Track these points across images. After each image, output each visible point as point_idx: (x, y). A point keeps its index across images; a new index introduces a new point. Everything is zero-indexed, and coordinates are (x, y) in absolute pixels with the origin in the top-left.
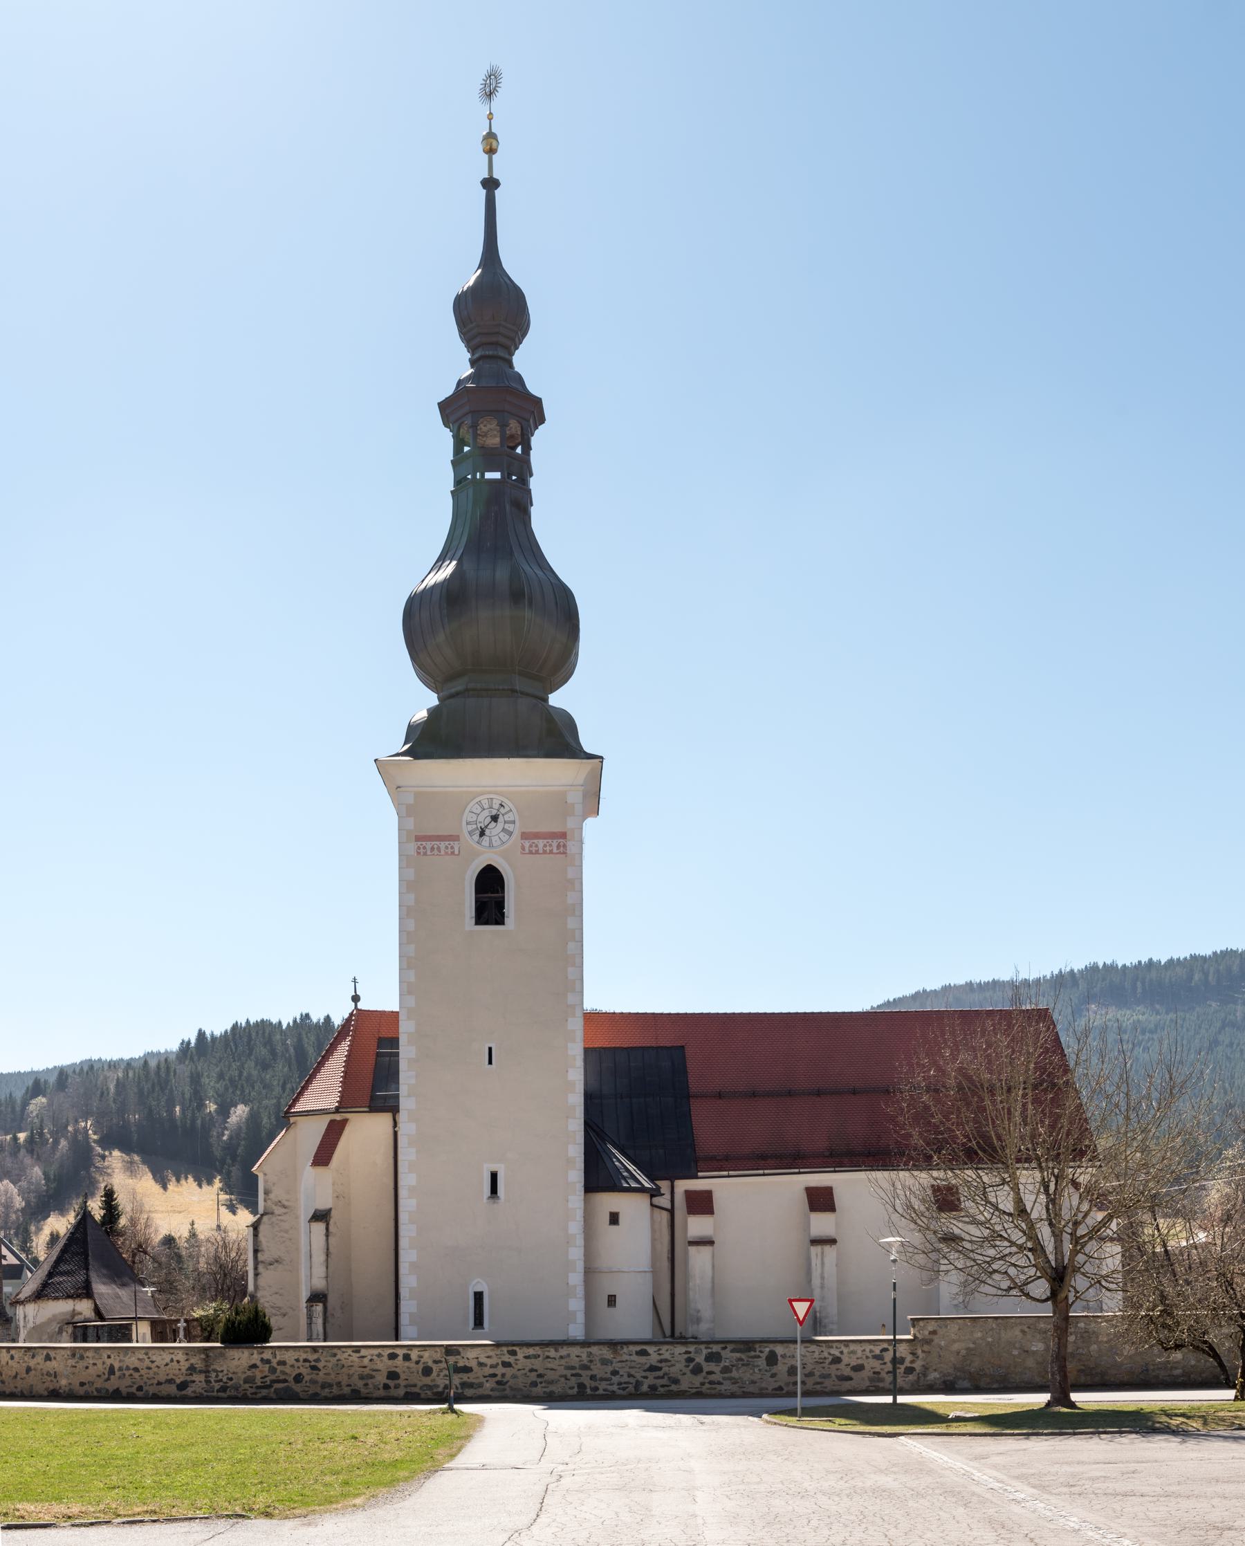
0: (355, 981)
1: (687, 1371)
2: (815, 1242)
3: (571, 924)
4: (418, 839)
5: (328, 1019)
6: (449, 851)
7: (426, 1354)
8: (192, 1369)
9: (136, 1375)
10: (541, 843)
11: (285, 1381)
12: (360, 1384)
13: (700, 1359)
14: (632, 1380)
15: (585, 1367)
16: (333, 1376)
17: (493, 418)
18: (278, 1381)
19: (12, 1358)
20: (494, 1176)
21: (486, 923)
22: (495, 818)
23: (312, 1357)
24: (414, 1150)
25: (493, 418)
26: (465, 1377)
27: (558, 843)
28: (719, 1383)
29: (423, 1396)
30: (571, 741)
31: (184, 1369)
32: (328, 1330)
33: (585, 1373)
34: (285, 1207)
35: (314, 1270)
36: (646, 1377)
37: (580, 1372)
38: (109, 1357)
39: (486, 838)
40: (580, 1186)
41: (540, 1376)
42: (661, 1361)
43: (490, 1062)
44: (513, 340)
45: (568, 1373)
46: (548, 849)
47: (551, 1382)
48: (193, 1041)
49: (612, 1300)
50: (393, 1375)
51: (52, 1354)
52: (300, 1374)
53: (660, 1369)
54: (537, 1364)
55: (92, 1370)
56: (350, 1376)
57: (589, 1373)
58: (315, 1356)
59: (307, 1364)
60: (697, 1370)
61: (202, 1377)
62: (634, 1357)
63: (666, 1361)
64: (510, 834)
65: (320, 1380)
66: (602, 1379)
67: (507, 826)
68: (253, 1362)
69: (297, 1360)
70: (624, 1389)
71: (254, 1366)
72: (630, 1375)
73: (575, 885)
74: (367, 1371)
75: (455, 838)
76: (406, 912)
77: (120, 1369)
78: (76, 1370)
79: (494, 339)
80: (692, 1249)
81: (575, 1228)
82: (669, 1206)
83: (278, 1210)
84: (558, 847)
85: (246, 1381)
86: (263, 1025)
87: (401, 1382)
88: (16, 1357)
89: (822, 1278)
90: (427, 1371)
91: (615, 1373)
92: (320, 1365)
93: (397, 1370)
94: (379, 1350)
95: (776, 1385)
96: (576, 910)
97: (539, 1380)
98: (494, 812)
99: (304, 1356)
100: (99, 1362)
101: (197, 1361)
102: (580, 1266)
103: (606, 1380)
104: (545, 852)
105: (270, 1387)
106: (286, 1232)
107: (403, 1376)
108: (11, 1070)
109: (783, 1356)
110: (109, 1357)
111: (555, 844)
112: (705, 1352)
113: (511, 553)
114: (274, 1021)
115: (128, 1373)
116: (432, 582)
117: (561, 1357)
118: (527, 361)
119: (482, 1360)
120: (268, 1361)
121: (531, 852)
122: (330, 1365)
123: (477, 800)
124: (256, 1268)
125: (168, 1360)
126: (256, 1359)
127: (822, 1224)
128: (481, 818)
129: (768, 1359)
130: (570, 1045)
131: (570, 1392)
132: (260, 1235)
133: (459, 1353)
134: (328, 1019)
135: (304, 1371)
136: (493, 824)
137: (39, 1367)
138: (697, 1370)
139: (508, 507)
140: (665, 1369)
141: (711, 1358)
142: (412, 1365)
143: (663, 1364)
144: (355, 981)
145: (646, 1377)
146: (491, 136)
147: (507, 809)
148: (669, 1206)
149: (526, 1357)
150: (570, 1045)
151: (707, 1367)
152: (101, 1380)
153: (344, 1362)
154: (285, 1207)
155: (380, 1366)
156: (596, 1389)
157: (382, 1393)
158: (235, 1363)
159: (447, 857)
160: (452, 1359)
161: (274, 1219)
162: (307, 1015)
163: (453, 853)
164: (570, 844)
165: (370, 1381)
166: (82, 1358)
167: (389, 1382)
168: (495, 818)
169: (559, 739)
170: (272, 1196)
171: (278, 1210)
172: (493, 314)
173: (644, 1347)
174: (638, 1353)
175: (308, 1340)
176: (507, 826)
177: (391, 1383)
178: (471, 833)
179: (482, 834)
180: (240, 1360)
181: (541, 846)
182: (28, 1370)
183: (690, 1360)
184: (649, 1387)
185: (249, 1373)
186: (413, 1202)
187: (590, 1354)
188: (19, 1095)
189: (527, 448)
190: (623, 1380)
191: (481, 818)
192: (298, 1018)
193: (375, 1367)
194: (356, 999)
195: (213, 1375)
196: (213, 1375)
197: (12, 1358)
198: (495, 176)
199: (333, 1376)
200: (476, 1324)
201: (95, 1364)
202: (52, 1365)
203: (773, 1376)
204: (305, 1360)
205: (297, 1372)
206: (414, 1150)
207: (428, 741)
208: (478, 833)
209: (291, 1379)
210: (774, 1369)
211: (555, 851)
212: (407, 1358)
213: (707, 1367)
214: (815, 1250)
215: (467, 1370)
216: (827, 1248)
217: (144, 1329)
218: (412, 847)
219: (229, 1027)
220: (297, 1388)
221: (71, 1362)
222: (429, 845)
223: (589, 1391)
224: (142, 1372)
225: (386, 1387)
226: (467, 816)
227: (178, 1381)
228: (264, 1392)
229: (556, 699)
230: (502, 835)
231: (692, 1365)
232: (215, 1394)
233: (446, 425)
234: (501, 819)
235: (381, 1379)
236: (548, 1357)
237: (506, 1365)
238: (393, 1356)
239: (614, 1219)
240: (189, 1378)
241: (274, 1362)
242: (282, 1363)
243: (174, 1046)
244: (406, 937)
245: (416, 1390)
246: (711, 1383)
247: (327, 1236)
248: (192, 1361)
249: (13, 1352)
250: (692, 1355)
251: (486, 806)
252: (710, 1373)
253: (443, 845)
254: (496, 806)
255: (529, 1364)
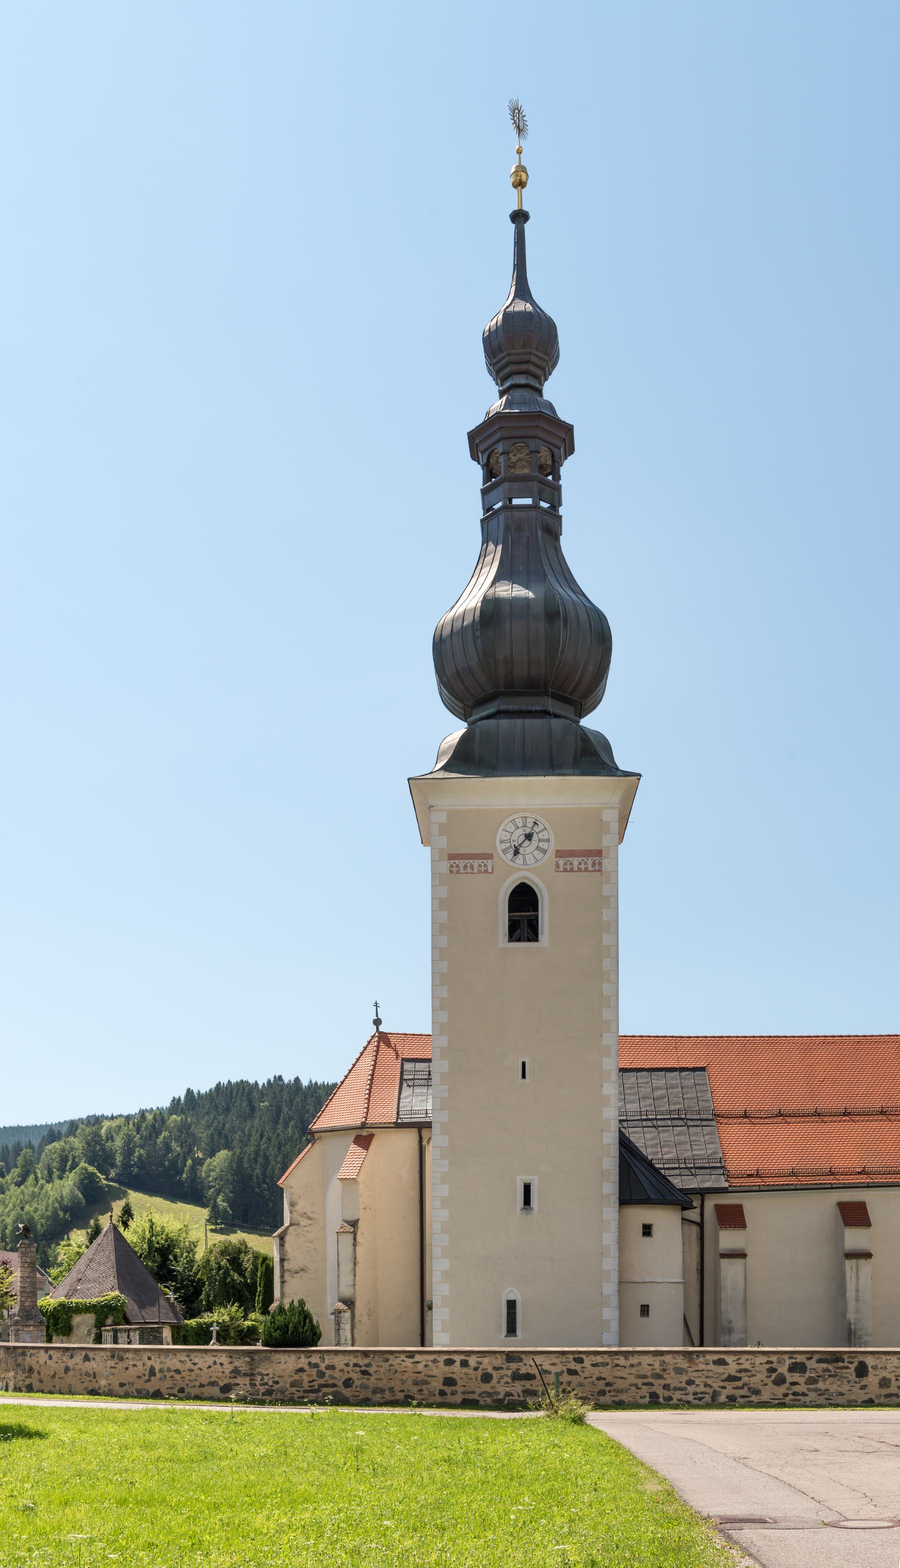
0: (376, 1005)
1: (769, 1381)
2: (850, 1255)
3: (606, 940)
4: (451, 857)
5: (297, 1080)
6: (483, 869)
7: (486, 1361)
8: (236, 1372)
9: (177, 1377)
10: (576, 861)
11: (334, 1385)
12: (414, 1390)
13: (783, 1369)
14: (708, 1390)
15: (659, 1377)
16: (385, 1382)
17: (522, 452)
18: (327, 1386)
19: (50, 1358)
20: (527, 1188)
21: (519, 940)
22: (529, 837)
23: (362, 1361)
24: (446, 1162)
25: (522, 452)
26: (528, 1384)
27: (591, 859)
28: (804, 1394)
29: (482, 1403)
30: (605, 758)
31: (227, 1372)
32: (356, 1336)
33: (656, 1382)
34: (310, 1218)
35: (342, 1279)
36: (724, 1388)
37: (652, 1381)
38: (149, 1358)
39: (520, 856)
40: (615, 1199)
41: (608, 1384)
42: (740, 1371)
43: (524, 1076)
44: (543, 369)
45: (640, 1382)
46: (583, 866)
47: (621, 1391)
48: (182, 1099)
49: (645, 1310)
50: (449, 1381)
51: (91, 1355)
52: (350, 1379)
53: (740, 1379)
54: (606, 1372)
55: (132, 1371)
56: (403, 1382)
57: (663, 1382)
58: (366, 1361)
59: (358, 1369)
60: (780, 1381)
61: (247, 1380)
62: (712, 1367)
63: (746, 1370)
64: (544, 852)
65: (371, 1386)
66: (676, 1389)
67: (541, 844)
68: (300, 1366)
69: (347, 1365)
70: (700, 1399)
71: (301, 1370)
72: (706, 1385)
73: (610, 902)
74: (421, 1377)
75: (489, 856)
76: (439, 929)
77: (161, 1371)
78: (115, 1371)
79: (524, 367)
80: (724, 1262)
81: (610, 1238)
82: (698, 1220)
83: (304, 1222)
84: (594, 864)
85: (293, 1385)
86: (243, 1084)
87: (459, 1389)
88: (54, 1357)
89: (857, 1291)
90: (487, 1378)
91: (690, 1382)
92: (371, 1370)
93: (454, 1376)
94: (435, 1356)
95: (867, 1398)
96: (612, 927)
97: (607, 1389)
98: (528, 831)
99: (355, 1361)
100: (140, 1364)
101: (241, 1364)
102: (614, 1277)
103: (681, 1389)
104: (580, 870)
105: (318, 1391)
106: (312, 1242)
107: (460, 1383)
108: (29, 1124)
109: (875, 1368)
110: (149, 1358)
111: (590, 861)
112: (788, 1362)
113: (545, 576)
114: (252, 1081)
115: (168, 1375)
116: (461, 610)
117: (632, 1365)
118: (560, 392)
119: (545, 1367)
120: (316, 1366)
121: (565, 870)
122: (382, 1370)
123: (510, 818)
124: (282, 1276)
125: (211, 1363)
126: (303, 1362)
127: (854, 1238)
128: (515, 837)
129: (856, 1370)
130: (604, 1060)
131: (642, 1401)
132: (286, 1245)
133: (521, 1360)
134: (297, 1080)
135: (354, 1376)
136: (527, 843)
137: (78, 1367)
138: (780, 1381)
139: (540, 534)
140: (745, 1379)
141: (793, 1368)
142: (471, 1371)
143: (743, 1374)
144: (376, 1005)
145: (724, 1388)
146: (521, 169)
147: (541, 827)
148: (698, 1220)
149: (593, 1365)
150: (604, 1060)
151: (790, 1377)
152: (141, 1381)
153: (397, 1367)
154: (310, 1218)
155: (435, 1372)
156: (670, 1398)
157: (438, 1399)
158: (282, 1366)
159: (481, 875)
160: (514, 1366)
161: (299, 1230)
162: (280, 1078)
163: (486, 871)
164: (605, 862)
165: (424, 1387)
166: (121, 1359)
167: (446, 1388)
168: (529, 837)
169: (592, 757)
170: (297, 1208)
171: (304, 1222)
172: (522, 348)
173: (722, 1356)
174: (715, 1362)
175: (336, 1345)
176: (541, 844)
177: (448, 1389)
178: (505, 851)
179: (517, 852)
180: (286, 1364)
181: (576, 863)
182: (67, 1370)
183: (772, 1370)
184: (728, 1397)
185: (296, 1377)
186: (444, 1214)
187: (663, 1363)
188: (36, 1143)
189: (557, 477)
190: (698, 1390)
191: (515, 837)
192: (272, 1079)
193: (431, 1373)
194: (377, 1022)
195: (259, 1378)
196: (259, 1378)
197: (50, 1358)
198: (524, 208)
199: (385, 1382)
200: (508, 1332)
201: (134, 1365)
202: (90, 1366)
203: (863, 1387)
204: (355, 1365)
205: (347, 1376)
206: (446, 1162)
207: (466, 759)
208: (512, 851)
209: (340, 1383)
210: (864, 1381)
211: (590, 868)
212: (464, 1364)
213: (790, 1377)
214: (849, 1264)
215: (529, 1377)
216: (862, 1262)
217: (167, 1333)
218: (445, 866)
219: (213, 1086)
220: (347, 1393)
221: (111, 1363)
222: (462, 863)
223: (661, 1400)
224: (183, 1374)
225: (442, 1393)
226: (501, 835)
227: (221, 1384)
228: (312, 1396)
229: (589, 722)
230: (536, 853)
231: (774, 1376)
232: (260, 1397)
233: (474, 457)
234: (535, 837)
235: (437, 1385)
236: (617, 1365)
237: (572, 1372)
238: (449, 1362)
239: (647, 1230)
240: (233, 1381)
241: (322, 1367)
242: (331, 1367)
243: (166, 1104)
244: (439, 954)
245: (475, 1397)
246: (794, 1394)
247: (355, 1246)
248: (237, 1364)
249: (51, 1352)
250: (774, 1365)
251: (520, 825)
252: (794, 1384)
253: (476, 863)
254: (530, 825)
255: (596, 1372)
